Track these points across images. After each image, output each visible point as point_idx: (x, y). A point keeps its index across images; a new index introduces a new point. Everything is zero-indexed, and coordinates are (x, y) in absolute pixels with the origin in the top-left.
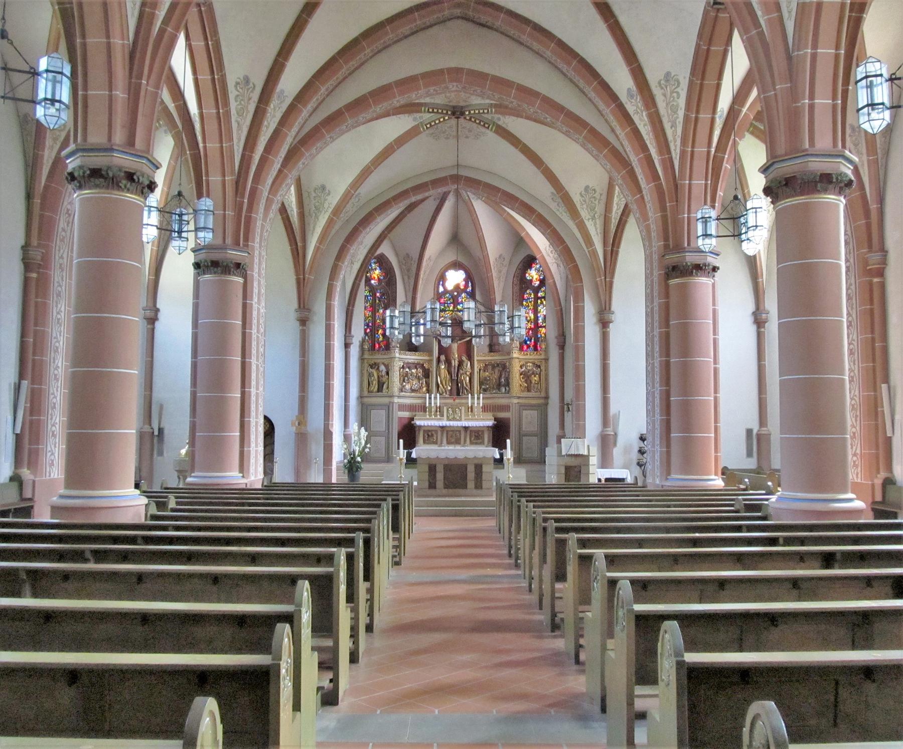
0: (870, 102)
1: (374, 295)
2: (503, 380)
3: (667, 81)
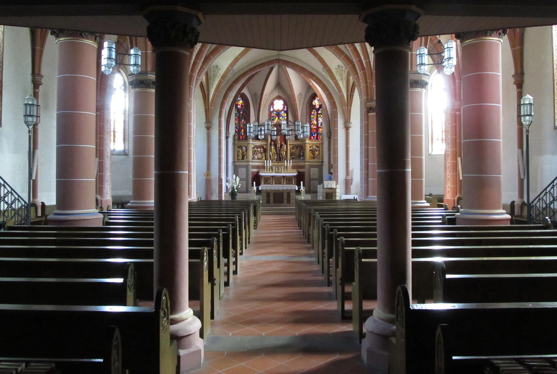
0: (421, 63)
1: (239, 113)
2: (301, 153)
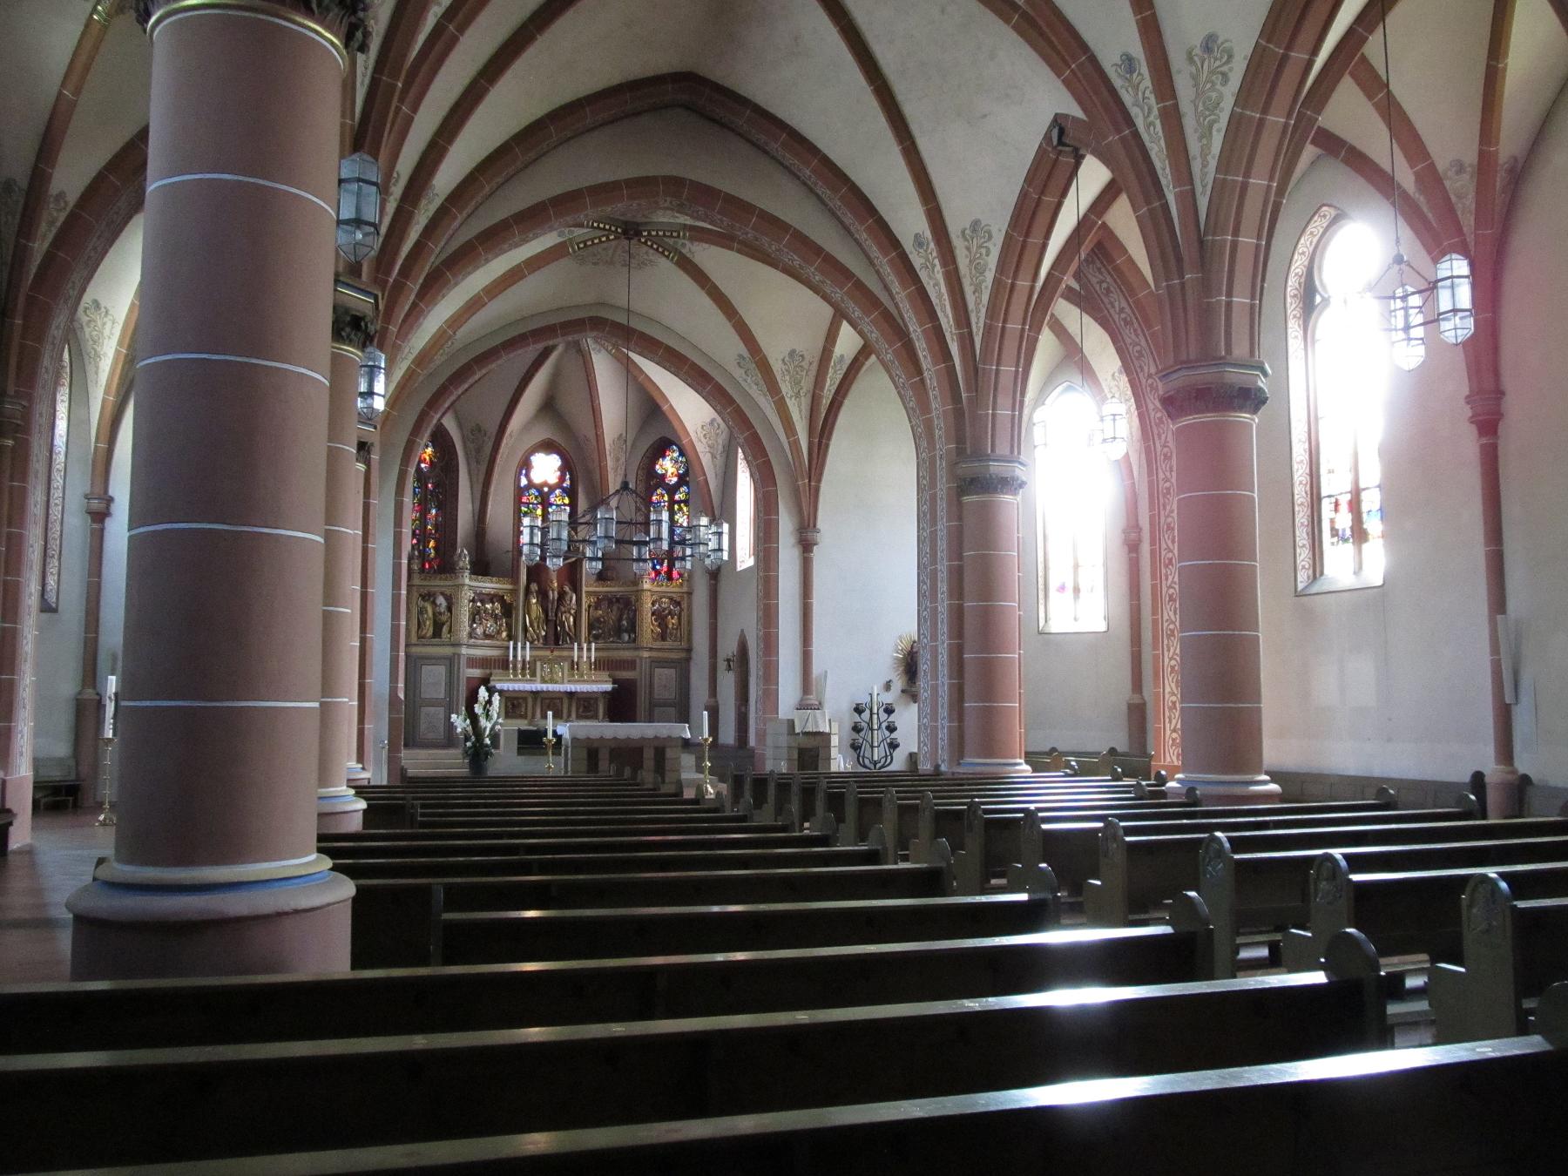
2: (625, 623)
3: (974, 231)
